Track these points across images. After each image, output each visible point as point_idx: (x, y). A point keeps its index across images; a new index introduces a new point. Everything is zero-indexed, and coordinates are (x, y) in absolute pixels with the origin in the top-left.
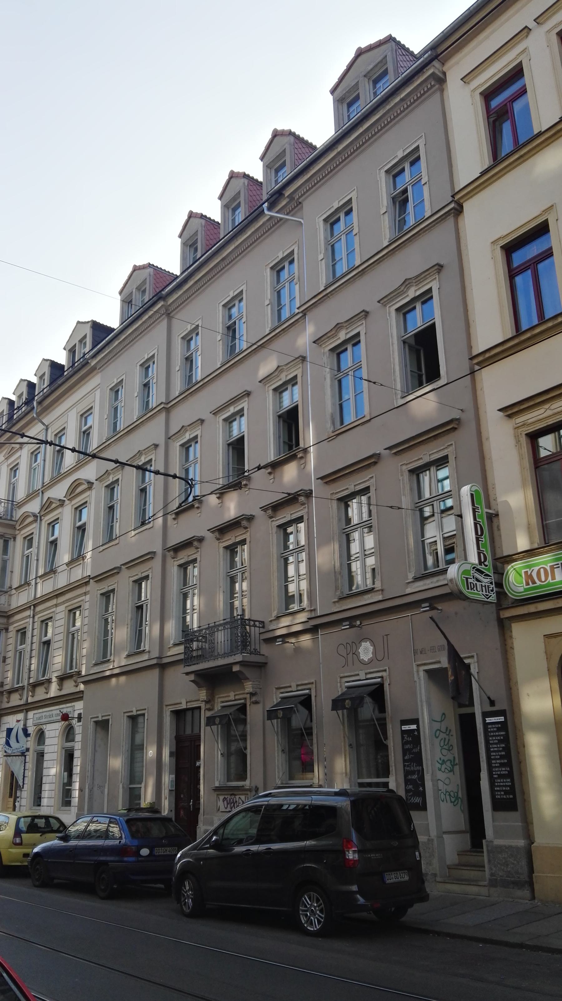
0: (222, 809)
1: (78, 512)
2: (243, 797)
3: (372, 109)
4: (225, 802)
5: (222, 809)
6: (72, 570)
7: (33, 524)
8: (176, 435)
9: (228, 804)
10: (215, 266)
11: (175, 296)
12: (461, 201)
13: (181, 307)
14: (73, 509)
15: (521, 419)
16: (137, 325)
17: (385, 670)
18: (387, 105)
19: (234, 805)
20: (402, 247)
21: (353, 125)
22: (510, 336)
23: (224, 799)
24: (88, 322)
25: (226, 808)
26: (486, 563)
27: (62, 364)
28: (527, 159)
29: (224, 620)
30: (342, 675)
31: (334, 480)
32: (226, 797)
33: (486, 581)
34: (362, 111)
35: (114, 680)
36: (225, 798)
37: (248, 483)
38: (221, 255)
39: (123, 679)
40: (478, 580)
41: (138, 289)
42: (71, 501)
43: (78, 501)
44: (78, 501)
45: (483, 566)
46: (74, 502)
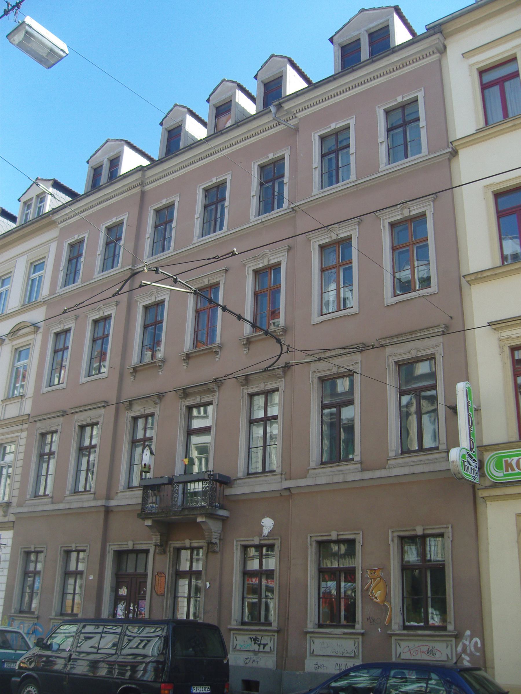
1: (18, 353)
6: (7, 406)
7: (31, 334)
12: (457, 148)
14: (14, 350)
15: (506, 333)
22: (498, 266)
24: (49, 180)
26: (474, 450)
27: (14, 215)
28: (467, 147)
33: (474, 464)
37: (219, 350)
40: (470, 464)
41: (38, 196)
42: (12, 341)
43: (18, 342)
44: (18, 342)
45: (472, 452)
46: (15, 343)
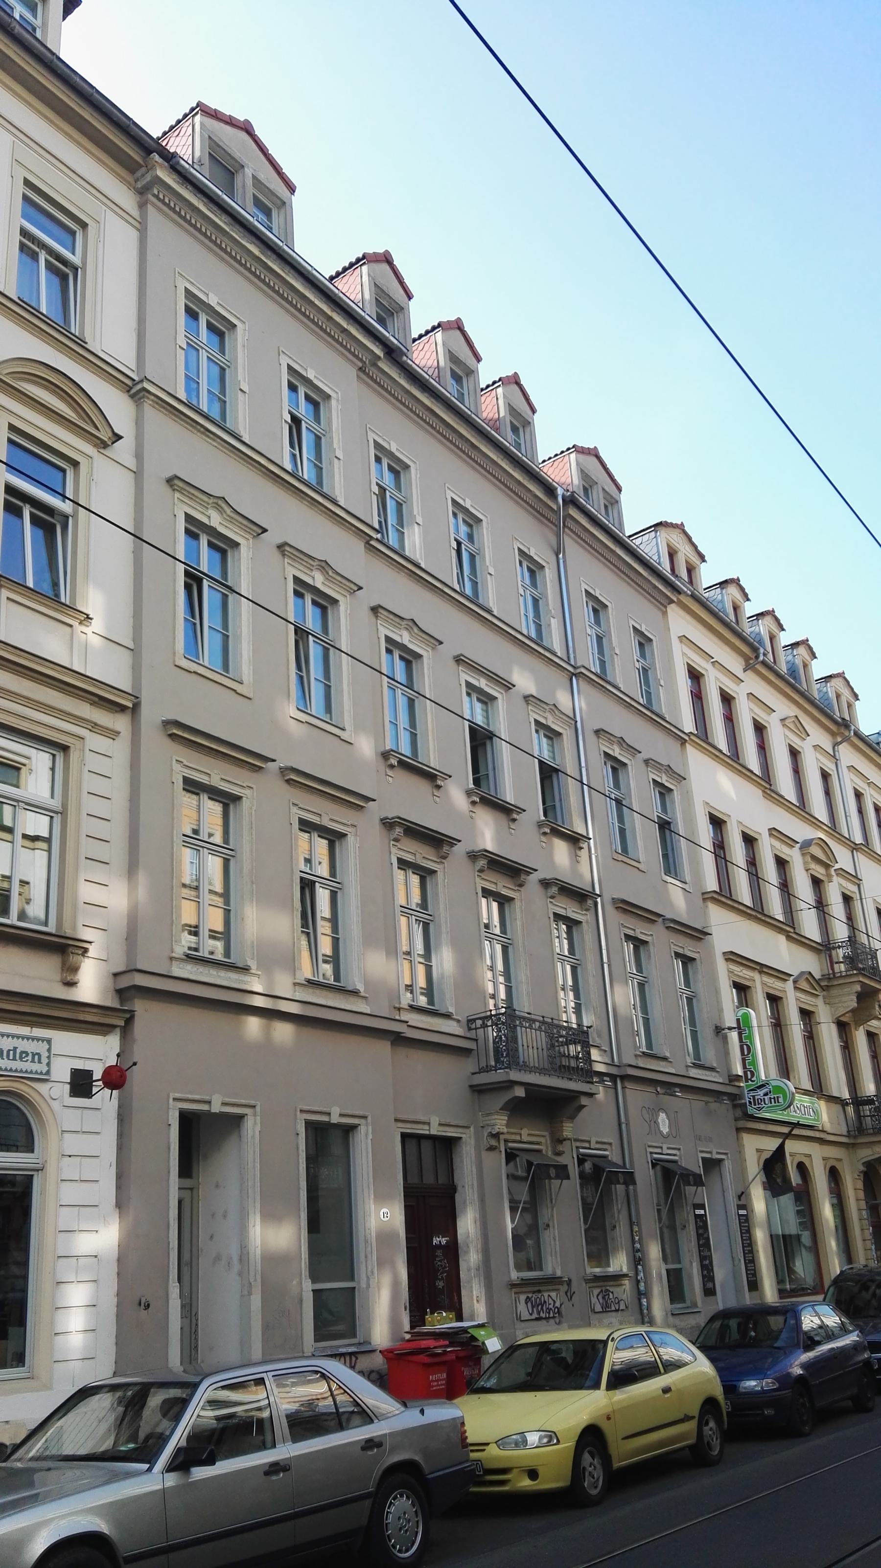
0: (525, 1315)
2: (553, 1294)
3: (191, 178)
4: (529, 1304)
5: (525, 1315)
8: (391, 617)
9: (533, 1307)
10: (461, 436)
11: (394, 373)
13: (509, 492)
16: (317, 302)
17: (679, 1149)
18: (372, 342)
19: (542, 1309)
20: (277, 481)
21: (327, 291)
23: (528, 1300)
25: (531, 1314)
29: (529, 1014)
30: (650, 1144)
31: (625, 911)
32: (530, 1295)
34: (314, 272)
35: (253, 1025)
36: (528, 1297)
38: (480, 442)
39: (284, 1031)
